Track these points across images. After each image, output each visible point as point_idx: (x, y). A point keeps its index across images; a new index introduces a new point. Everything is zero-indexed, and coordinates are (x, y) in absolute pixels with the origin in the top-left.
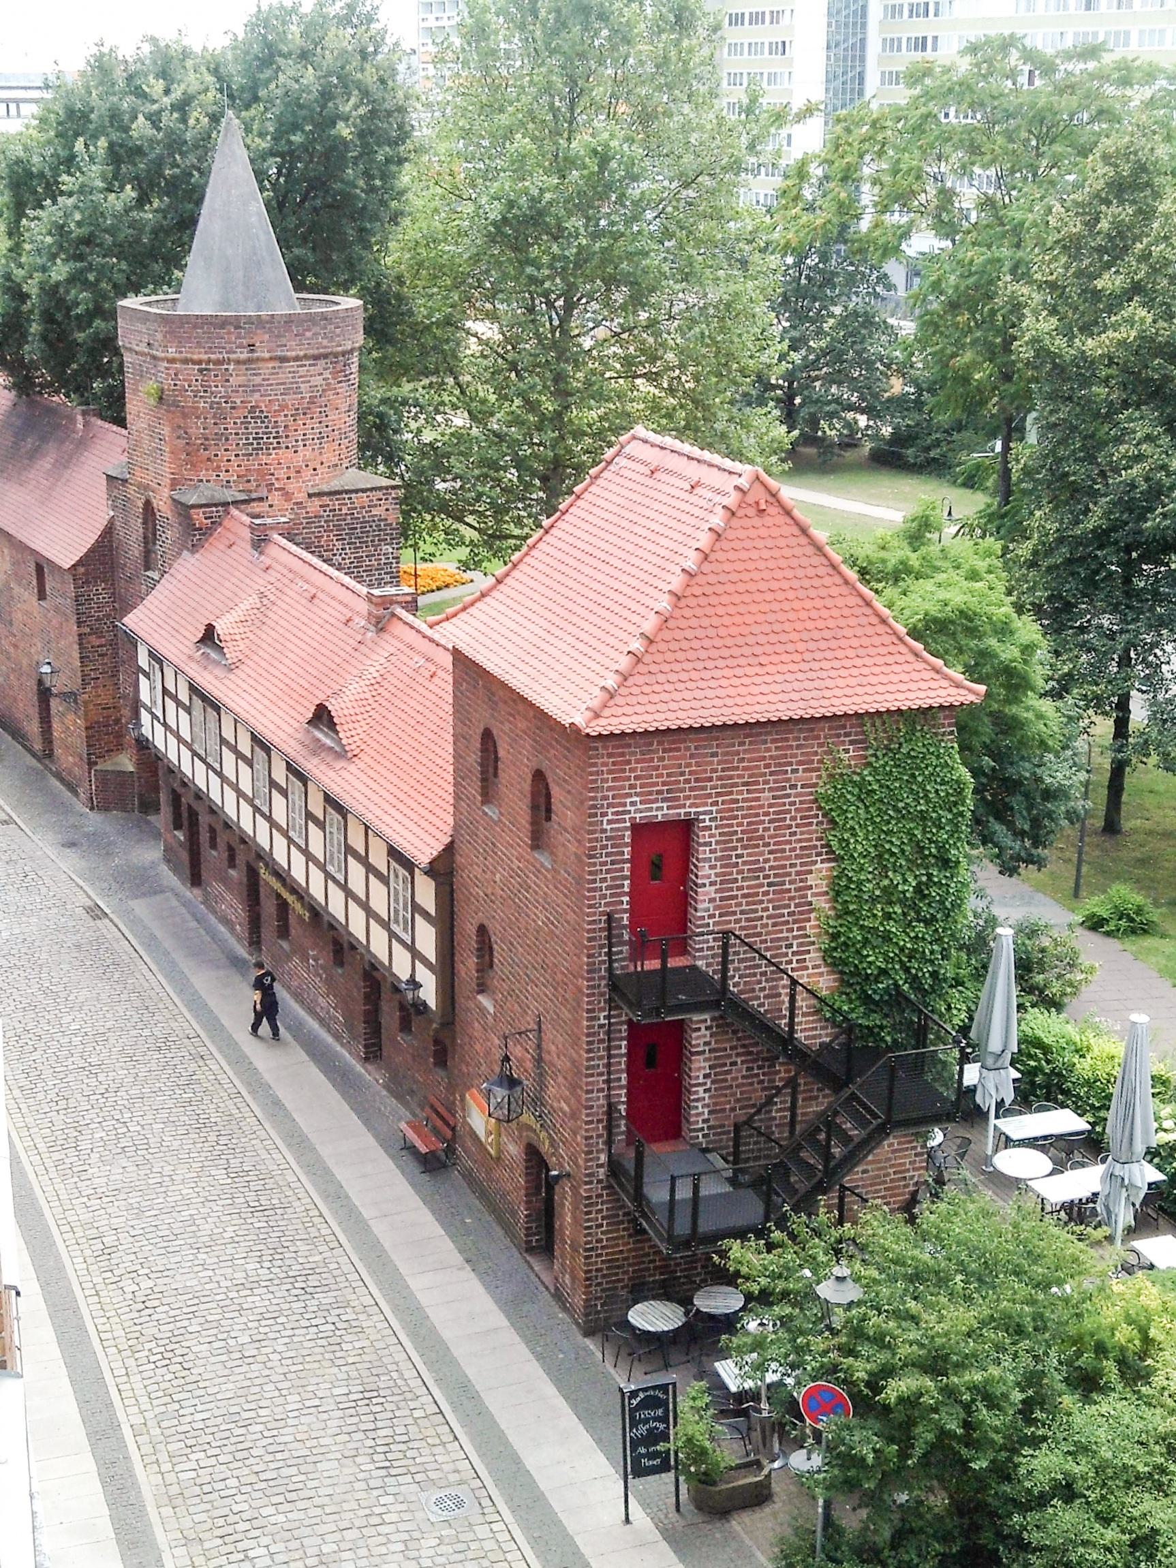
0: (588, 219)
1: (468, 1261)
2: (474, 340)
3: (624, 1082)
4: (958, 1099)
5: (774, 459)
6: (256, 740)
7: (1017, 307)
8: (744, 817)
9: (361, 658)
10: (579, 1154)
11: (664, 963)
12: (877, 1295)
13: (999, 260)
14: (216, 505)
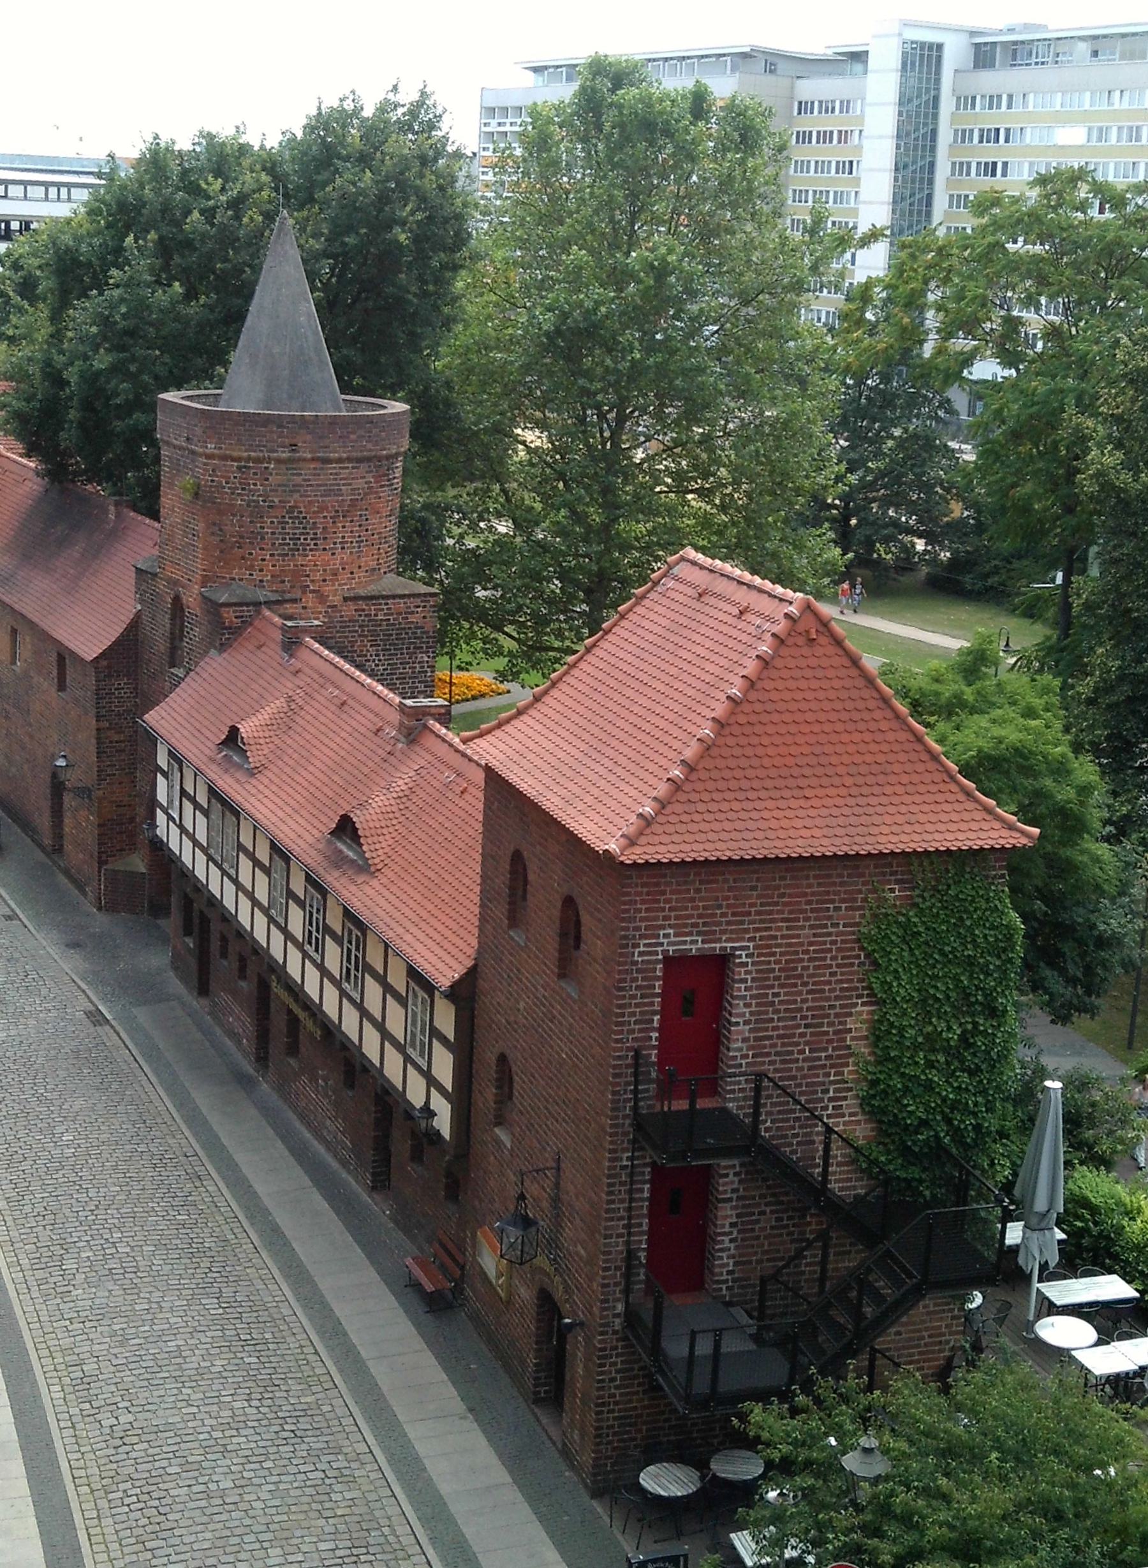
0: (645, 333)
1: (471, 1410)
2: (521, 447)
3: (645, 1228)
4: (999, 1259)
5: (826, 581)
6: (275, 848)
7: (1081, 439)
8: (781, 954)
9: (390, 769)
10: (595, 1303)
11: (692, 1104)
12: (906, 1470)
13: (1062, 391)
14: (247, 605)
